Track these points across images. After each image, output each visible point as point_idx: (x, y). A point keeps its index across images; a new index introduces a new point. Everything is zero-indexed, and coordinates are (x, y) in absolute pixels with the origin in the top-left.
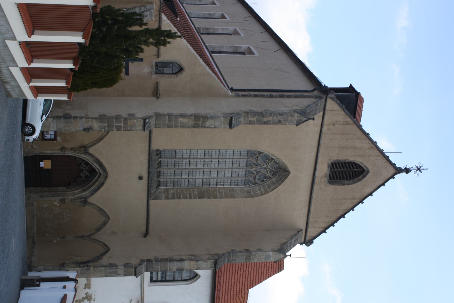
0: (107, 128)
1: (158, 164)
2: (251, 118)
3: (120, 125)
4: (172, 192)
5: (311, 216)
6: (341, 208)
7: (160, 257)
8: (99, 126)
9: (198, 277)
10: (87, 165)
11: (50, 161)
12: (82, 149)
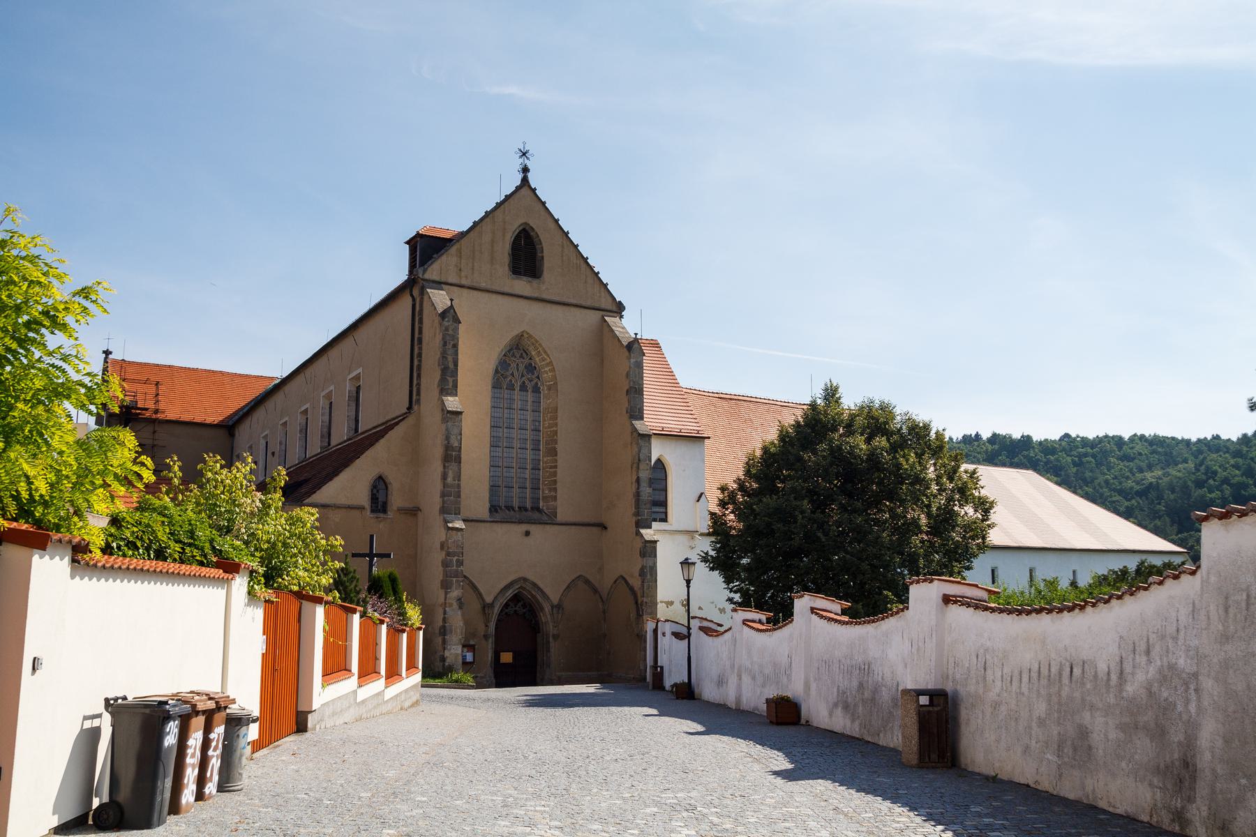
1: (509, 510)
2: (448, 385)
6: (575, 261)
7: (634, 508)
8: (456, 589)
10: (509, 605)
11: (501, 653)
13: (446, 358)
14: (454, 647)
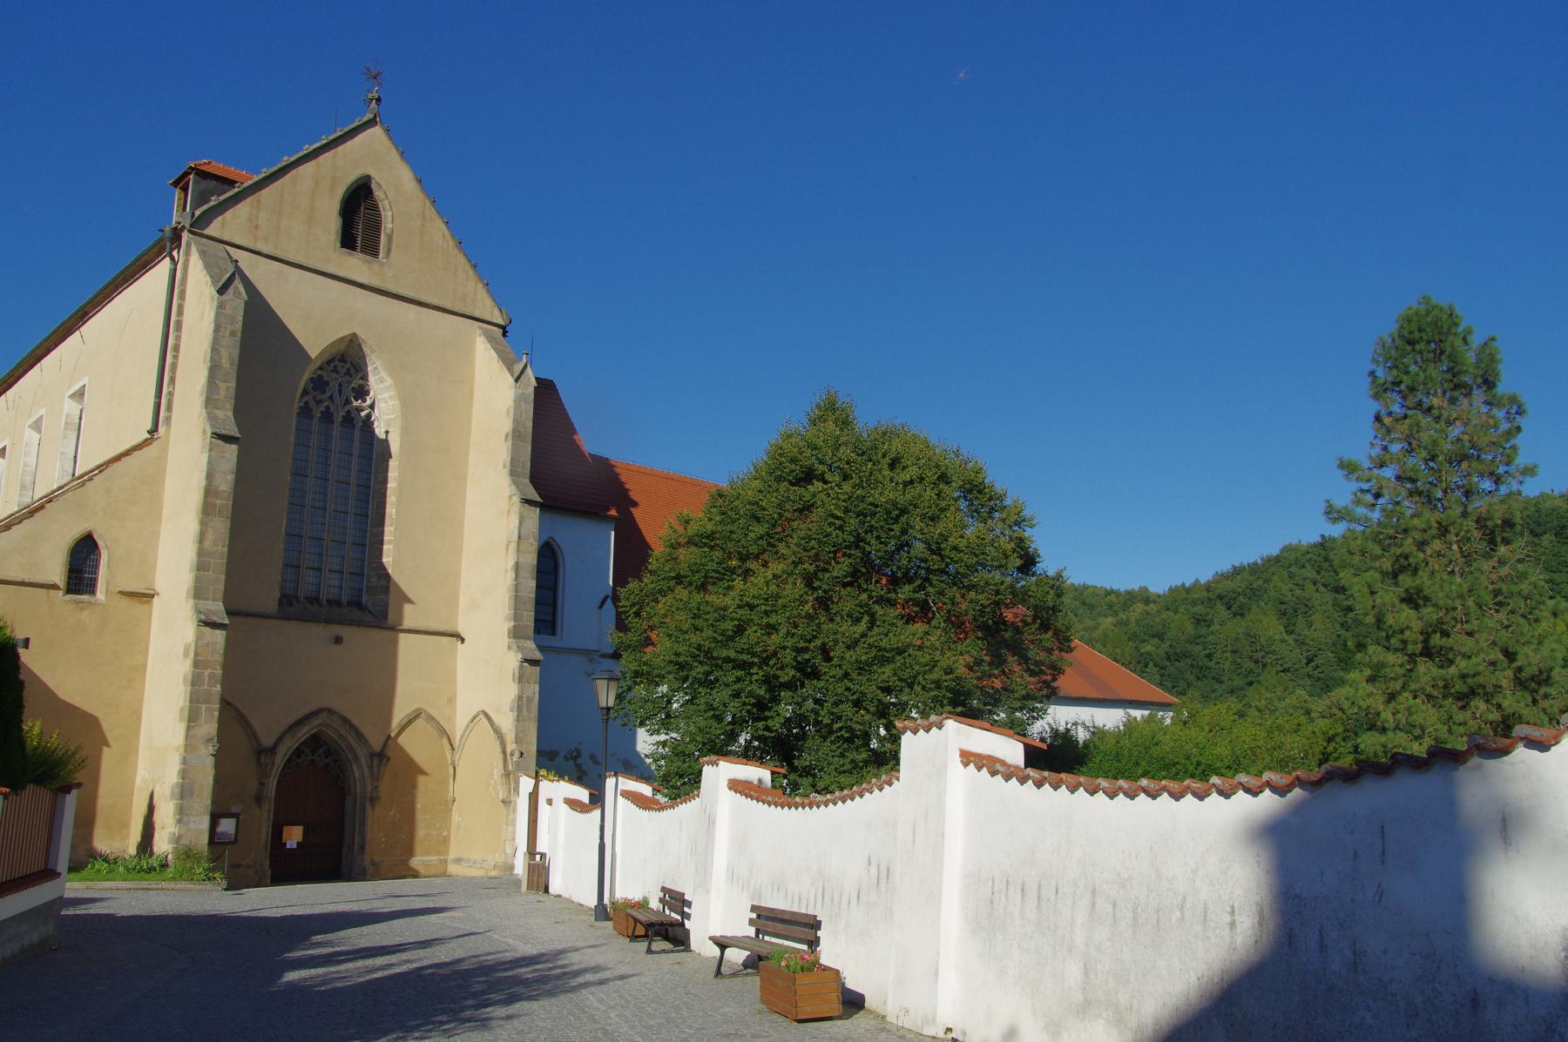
0: (213, 706)
1: (311, 603)
2: (218, 394)
3: (209, 676)
4: (374, 579)
5: (448, 306)
6: (441, 244)
8: (206, 722)
9: (551, 541)
10: (302, 752)
11: (285, 828)
12: (262, 760)
13: (578, 1010)
14: (195, 818)
